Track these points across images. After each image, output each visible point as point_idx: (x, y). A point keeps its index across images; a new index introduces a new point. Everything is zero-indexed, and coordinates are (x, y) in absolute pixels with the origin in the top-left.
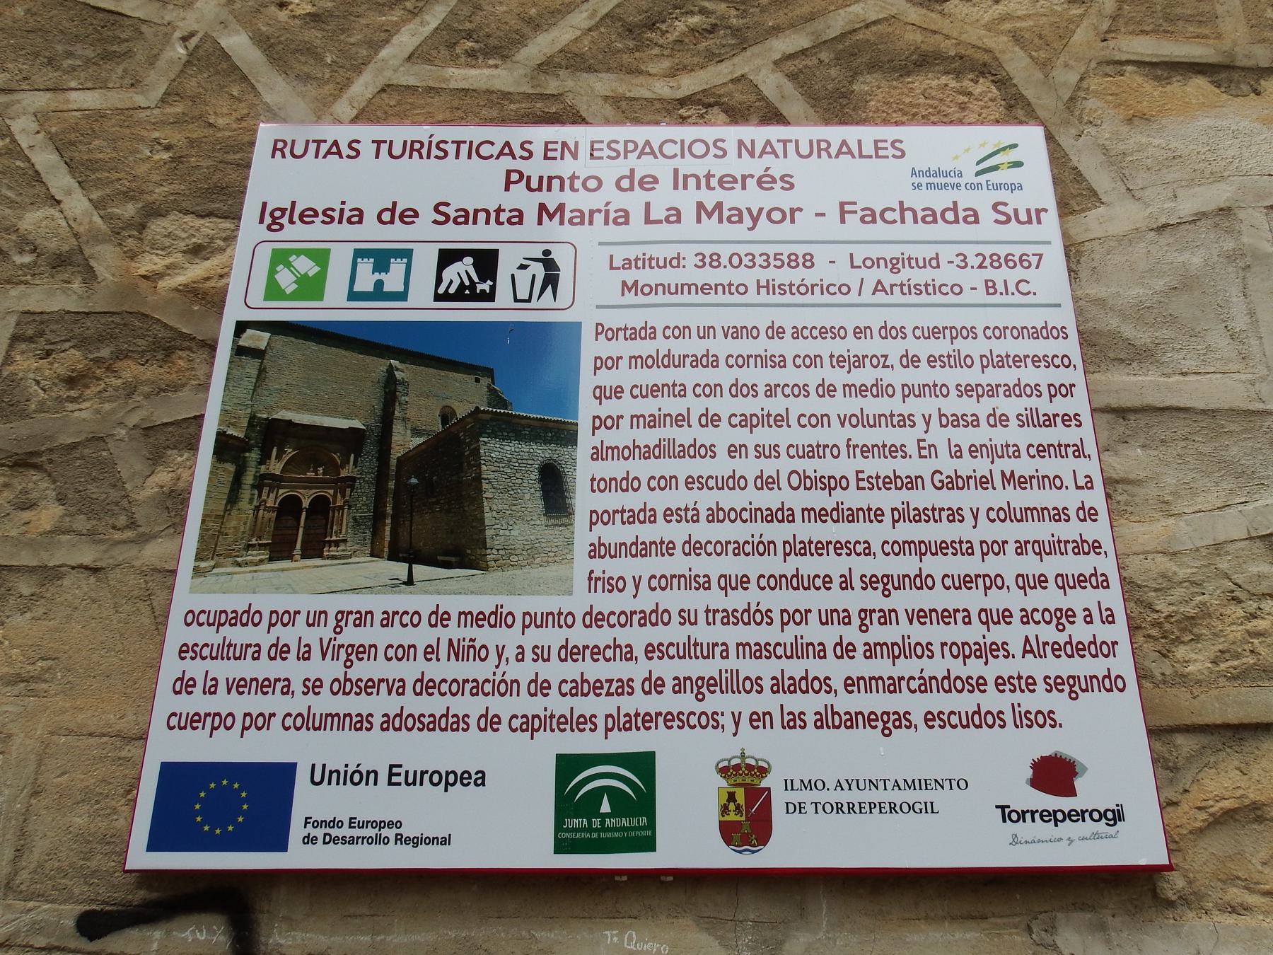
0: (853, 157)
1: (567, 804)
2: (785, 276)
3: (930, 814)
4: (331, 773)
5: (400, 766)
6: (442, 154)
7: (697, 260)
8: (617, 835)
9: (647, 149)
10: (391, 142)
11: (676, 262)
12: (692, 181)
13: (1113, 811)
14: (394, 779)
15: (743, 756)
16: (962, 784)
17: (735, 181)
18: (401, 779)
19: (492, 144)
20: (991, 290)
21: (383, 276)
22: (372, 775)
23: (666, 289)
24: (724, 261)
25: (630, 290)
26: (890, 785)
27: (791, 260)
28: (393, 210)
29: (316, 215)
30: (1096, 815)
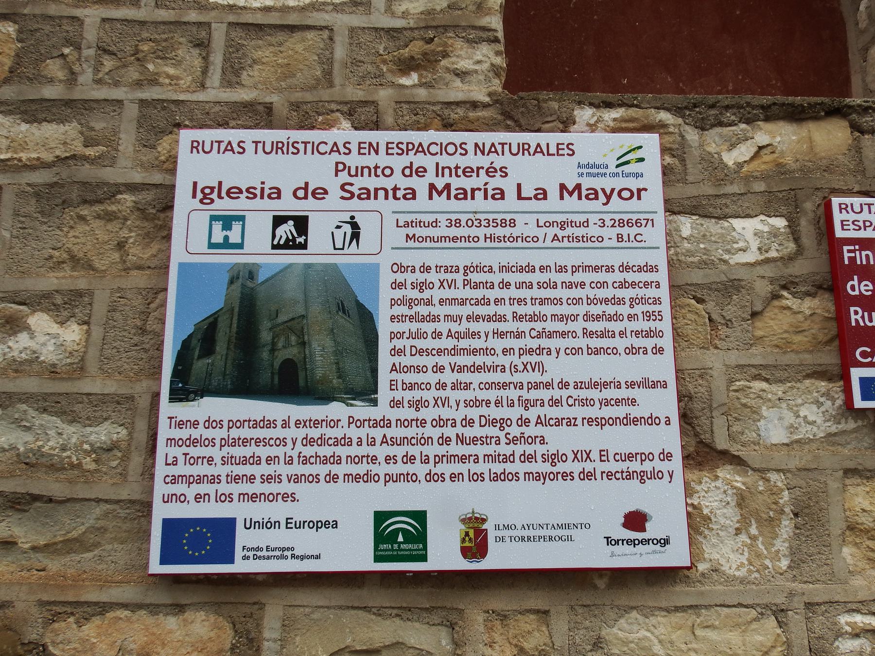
0: (544, 155)
1: (380, 538)
2: (500, 231)
3: (570, 542)
4: (255, 523)
5: (292, 519)
6: (295, 151)
7: (447, 223)
8: (407, 553)
9: (420, 149)
10: (264, 142)
11: (435, 224)
12: (447, 171)
13: (664, 539)
14: (289, 525)
15: (473, 512)
16: (587, 526)
17: (473, 171)
18: (293, 525)
19: (326, 144)
20: (620, 240)
21: (228, 233)
22: (277, 524)
23: (432, 239)
24: (463, 223)
25: (411, 239)
26: (549, 527)
27: (502, 223)
28: (306, 188)
29: (241, 192)
30: (655, 542)
